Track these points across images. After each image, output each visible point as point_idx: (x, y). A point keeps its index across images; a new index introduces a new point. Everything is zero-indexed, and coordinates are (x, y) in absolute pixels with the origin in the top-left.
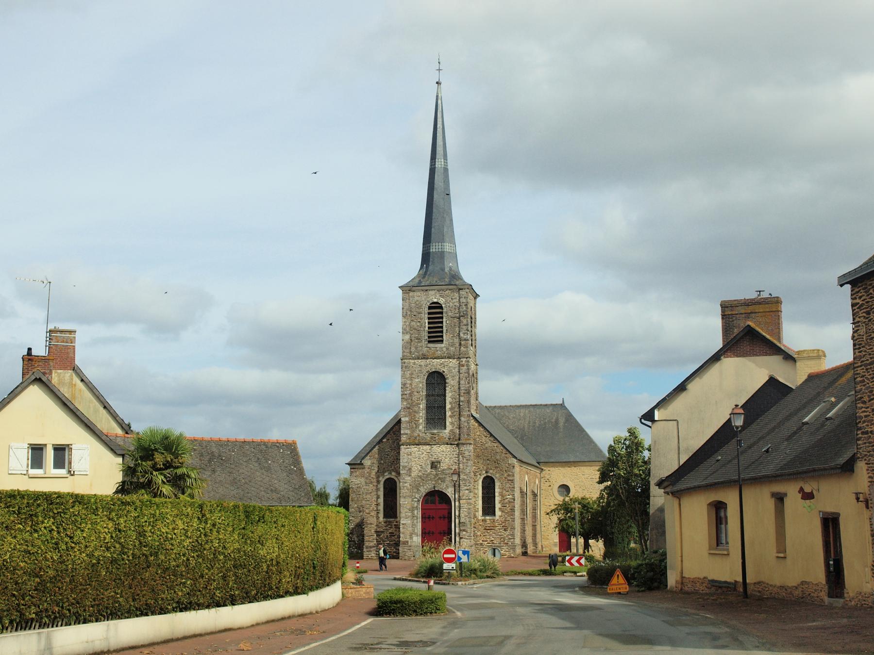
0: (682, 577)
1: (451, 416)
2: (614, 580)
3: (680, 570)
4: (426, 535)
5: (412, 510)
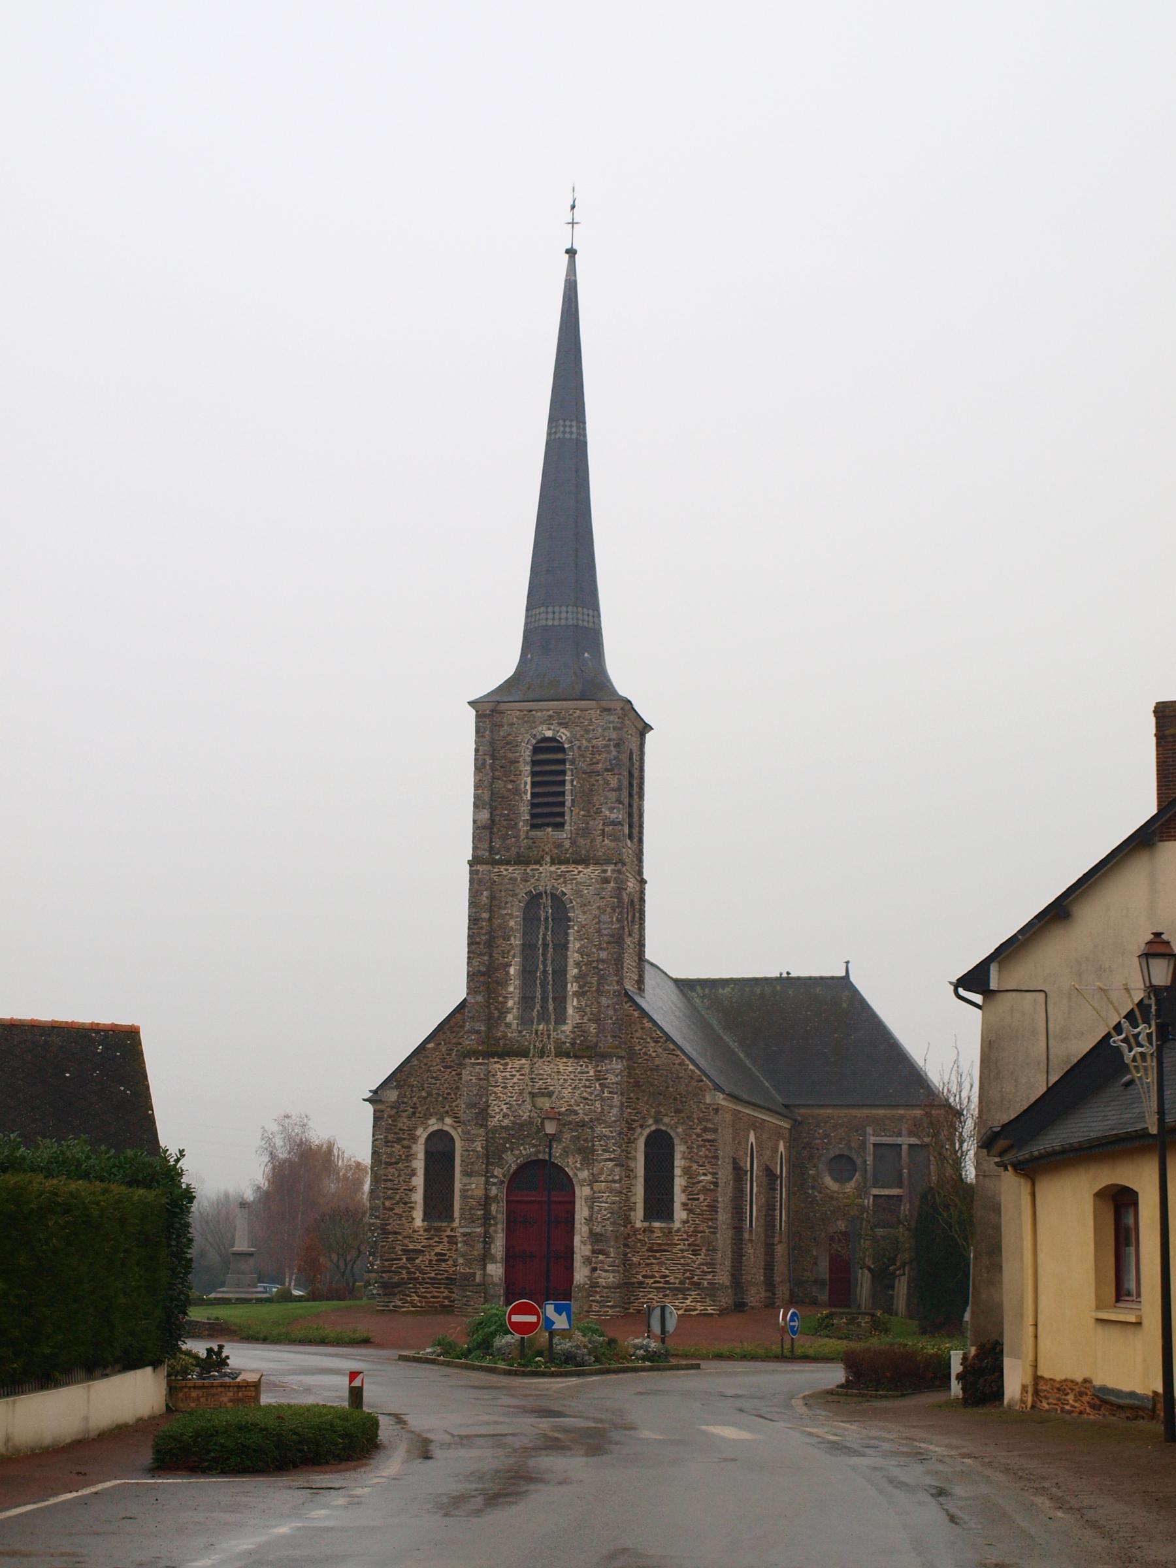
0: (1037, 1379)
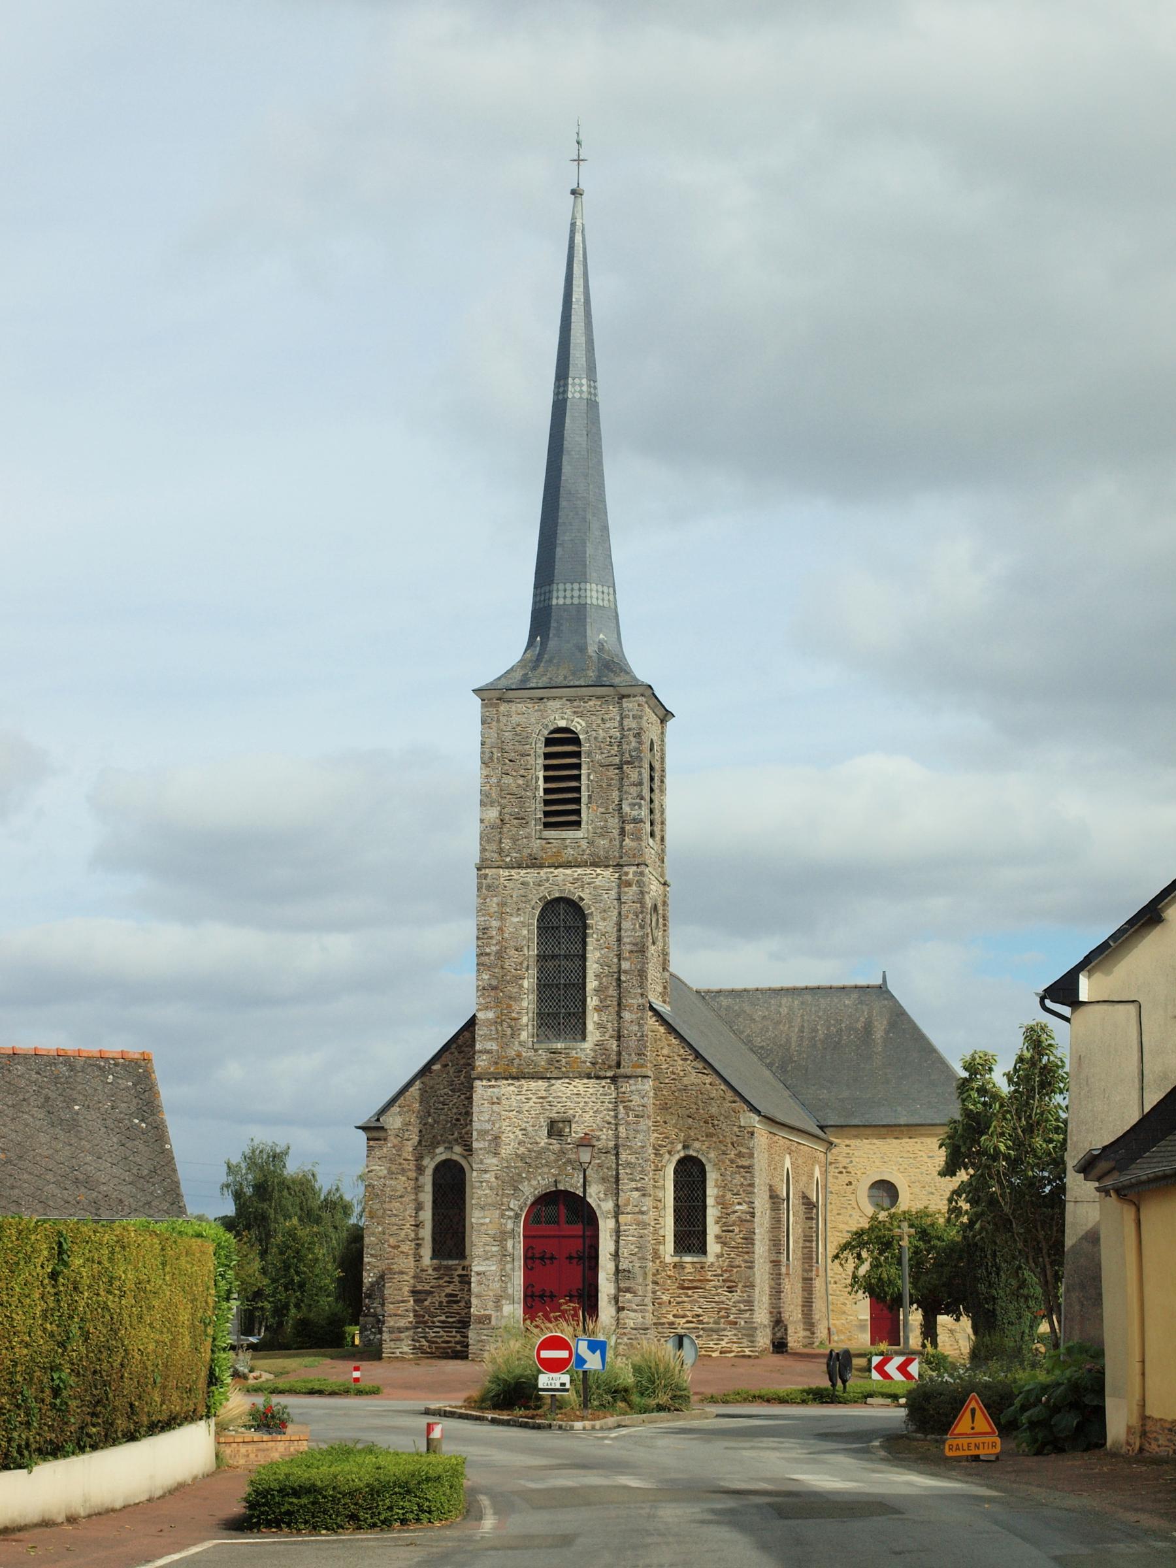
0: (1144, 1418)
1: (598, 1009)
2: (963, 1424)
3: (1137, 1396)
4: (538, 1301)
5: (502, 1237)
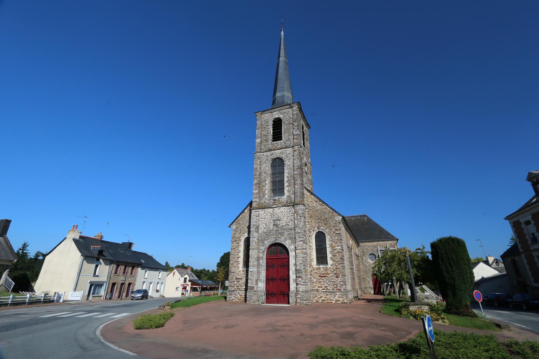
5: (258, 259)
